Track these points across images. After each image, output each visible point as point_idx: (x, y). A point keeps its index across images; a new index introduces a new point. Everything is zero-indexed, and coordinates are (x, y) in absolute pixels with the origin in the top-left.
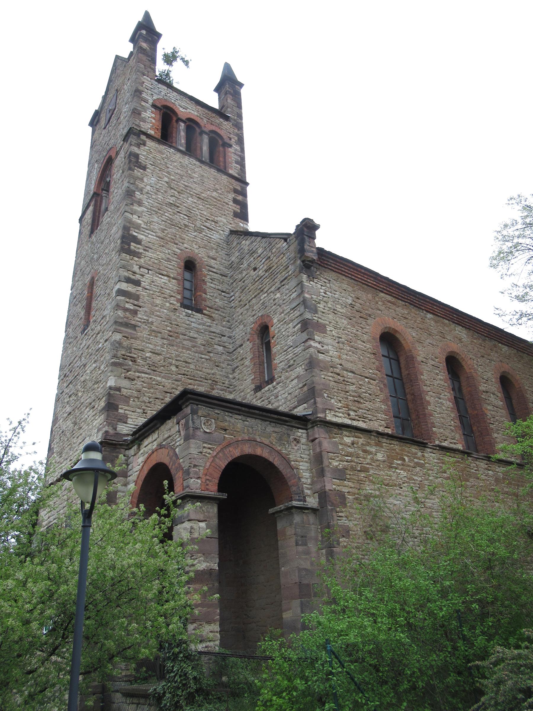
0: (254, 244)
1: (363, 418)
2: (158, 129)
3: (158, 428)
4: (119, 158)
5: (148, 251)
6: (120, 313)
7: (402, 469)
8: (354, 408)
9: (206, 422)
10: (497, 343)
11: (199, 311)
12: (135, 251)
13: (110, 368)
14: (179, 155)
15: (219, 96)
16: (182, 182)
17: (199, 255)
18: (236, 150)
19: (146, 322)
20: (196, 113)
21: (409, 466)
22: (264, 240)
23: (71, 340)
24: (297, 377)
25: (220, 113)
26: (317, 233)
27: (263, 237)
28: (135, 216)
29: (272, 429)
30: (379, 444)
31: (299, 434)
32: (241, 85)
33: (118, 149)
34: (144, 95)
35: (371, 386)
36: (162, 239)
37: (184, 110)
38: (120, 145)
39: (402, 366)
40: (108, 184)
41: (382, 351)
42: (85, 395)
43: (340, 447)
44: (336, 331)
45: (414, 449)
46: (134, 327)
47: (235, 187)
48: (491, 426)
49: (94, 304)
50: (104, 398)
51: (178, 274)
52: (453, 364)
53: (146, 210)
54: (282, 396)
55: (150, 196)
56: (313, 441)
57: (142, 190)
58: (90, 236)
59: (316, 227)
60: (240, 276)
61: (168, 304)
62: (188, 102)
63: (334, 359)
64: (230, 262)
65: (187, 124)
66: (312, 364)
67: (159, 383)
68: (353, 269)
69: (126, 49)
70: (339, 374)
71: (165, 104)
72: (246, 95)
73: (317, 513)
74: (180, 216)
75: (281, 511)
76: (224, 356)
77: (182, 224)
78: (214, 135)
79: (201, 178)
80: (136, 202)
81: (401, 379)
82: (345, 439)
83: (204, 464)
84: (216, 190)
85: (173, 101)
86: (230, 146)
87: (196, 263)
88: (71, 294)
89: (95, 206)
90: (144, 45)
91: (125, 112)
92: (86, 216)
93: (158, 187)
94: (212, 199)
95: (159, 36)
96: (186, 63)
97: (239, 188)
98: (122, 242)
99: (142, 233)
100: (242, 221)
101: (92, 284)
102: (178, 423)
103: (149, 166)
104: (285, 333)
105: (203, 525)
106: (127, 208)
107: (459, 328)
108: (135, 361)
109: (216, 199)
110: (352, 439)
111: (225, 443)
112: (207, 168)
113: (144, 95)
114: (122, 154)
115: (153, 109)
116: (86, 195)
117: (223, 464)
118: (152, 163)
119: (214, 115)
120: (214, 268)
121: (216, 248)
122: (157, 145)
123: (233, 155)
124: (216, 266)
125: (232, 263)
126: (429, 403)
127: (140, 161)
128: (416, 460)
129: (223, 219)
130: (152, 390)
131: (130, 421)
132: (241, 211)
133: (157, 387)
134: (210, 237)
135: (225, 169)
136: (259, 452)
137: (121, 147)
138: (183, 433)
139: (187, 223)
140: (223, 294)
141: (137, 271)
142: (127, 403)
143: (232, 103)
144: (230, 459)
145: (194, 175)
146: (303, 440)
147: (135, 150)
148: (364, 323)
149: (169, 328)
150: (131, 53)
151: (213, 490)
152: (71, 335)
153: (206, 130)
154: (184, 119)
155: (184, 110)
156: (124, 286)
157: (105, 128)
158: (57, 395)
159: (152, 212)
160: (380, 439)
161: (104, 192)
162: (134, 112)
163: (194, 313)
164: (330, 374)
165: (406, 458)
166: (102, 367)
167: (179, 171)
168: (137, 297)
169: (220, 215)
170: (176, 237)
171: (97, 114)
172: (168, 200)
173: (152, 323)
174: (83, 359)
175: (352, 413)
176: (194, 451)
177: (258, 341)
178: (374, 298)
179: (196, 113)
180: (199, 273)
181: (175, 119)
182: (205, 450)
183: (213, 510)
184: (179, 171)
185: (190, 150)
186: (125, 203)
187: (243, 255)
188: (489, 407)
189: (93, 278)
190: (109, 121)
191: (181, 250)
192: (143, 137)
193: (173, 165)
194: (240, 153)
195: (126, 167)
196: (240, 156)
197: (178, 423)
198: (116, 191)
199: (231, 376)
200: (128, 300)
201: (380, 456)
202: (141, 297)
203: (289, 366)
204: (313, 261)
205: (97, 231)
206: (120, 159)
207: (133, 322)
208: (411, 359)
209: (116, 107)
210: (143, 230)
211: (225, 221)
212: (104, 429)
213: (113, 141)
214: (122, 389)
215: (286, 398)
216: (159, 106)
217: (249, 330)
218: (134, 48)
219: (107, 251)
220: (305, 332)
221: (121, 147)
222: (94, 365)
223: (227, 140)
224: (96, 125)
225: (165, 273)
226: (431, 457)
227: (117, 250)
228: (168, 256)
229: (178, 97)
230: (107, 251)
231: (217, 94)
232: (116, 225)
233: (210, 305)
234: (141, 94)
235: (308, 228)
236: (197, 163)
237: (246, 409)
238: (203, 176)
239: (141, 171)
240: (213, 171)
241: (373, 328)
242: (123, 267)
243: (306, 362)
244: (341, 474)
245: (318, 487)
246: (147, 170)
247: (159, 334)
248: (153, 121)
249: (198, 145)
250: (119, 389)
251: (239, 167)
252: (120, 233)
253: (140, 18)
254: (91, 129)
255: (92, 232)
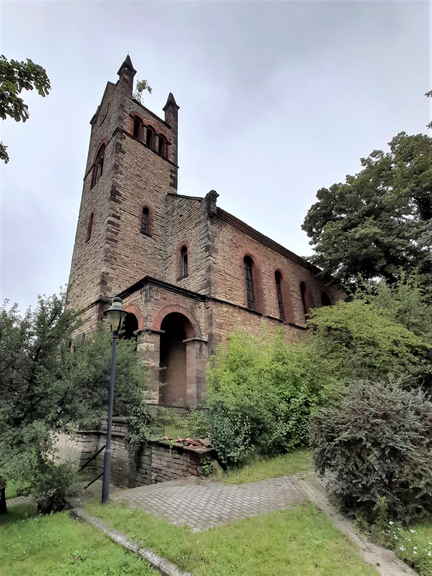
0: (182, 202)
1: (233, 299)
3: (129, 295)
4: (109, 145)
6: (110, 233)
7: (249, 326)
8: (229, 294)
9: (158, 294)
10: (301, 266)
11: (150, 236)
13: (103, 262)
14: (142, 147)
15: (165, 113)
18: (173, 147)
19: (122, 239)
20: (153, 123)
21: (253, 325)
22: (187, 200)
23: (79, 246)
24: (201, 275)
25: (165, 124)
26: (218, 199)
27: (187, 199)
28: (118, 180)
29: (188, 301)
30: (239, 313)
31: (201, 304)
32: (178, 108)
35: (238, 283)
37: (148, 121)
39: (253, 274)
40: (102, 160)
41: (243, 265)
42: (88, 275)
43: (221, 312)
44: (223, 252)
45: (256, 317)
46: (116, 241)
48: (294, 309)
49: (93, 227)
50: (100, 278)
51: (140, 215)
52: (278, 275)
54: (193, 284)
56: (207, 308)
58: (91, 189)
59: (218, 195)
60: (172, 219)
61: (134, 231)
63: (221, 268)
66: (209, 269)
67: (128, 272)
68: (234, 220)
69: (115, 79)
70: (222, 276)
72: (182, 115)
73: (207, 344)
75: (189, 342)
76: (161, 261)
81: (252, 281)
82: (224, 308)
83: (155, 315)
84: (161, 169)
86: (170, 144)
88: (79, 220)
89: (94, 172)
90: (126, 77)
92: (88, 177)
95: (135, 72)
96: (150, 90)
97: (174, 170)
98: (111, 194)
101: (92, 216)
102: (141, 294)
103: (126, 152)
104: (196, 252)
105: (152, 345)
107: (283, 257)
108: (116, 260)
110: (227, 309)
111: (164, 306)
112: (157, 156)
113: (125, 108)
114: (111, 143)
117: (163, 316)
119: (162, 124)
123: (171, 149)
124: (159, 212)
126: (265, 294)
128: (256, 322)
130: (124, 276)
131: (112, 291)
133: (127, 274)
136: (181, 311)
137: (111, 139)
138: (143, 299)
139: (145, 187)
140: (162, 228)
141: (119, 211)
142: (112, 282)
143: (173, 118)
144: (167, 314)
146: (203, 308)
147: (120, 142)
148: (237, 250)
149: (134, 244)
150: (118, 82)
151: (158, 328)
152: (79, 243)
154: (146, 125)
155: (147, 120)
156: (112, 219)
157: (100, 126)
158: (70, 274)
160: (240, 310)
163: (147, 237)
164: (219, 275)
165: (252, 321)
166: (98, 261)
168: (118, 226)
171: (95, 117)
173: (125, 240)
174: (86, 256)
175: (228, 296)
176: (149, 308)
177: (180, 255)
178: (243, 237)
179: (153, 123)
180: (150, 215)
181: (141, 125)
182: (155, 308)
183: (157, 338)
185: (149, 145)
187: (175, 208)
188: (293, 299)
189: (93, 213)
192: (124, 134)
197: (141, 294)
198: (107, 164)
199: (164, 272)
200: (113, 227)
201: (239, 319)
202: (120, 226)
203: (197, 269)
204: (214, 214)
207: (116, 239)
208: (258, 271)
212: (100, 294)
214: (110, 274)
215: (194, 285)
216: (133, 115)
217: (175, 248)
218: (120, 78)
219: (101, 198)
220: (207, 252)
221: (111, 139)
222: (94, 260)
223: (169, 141)
224: (94, 124)
225: (133, 214)
226: (264, 321)
229: (144, 112)
233: (155, 233)
235: (213, 196)
236: (152, 152)
237: (176, 289)
238: (155, 160)
240: (160, 158)
241: (241, 254)
242: (112, 208)
243: (207, 268)
244: (220, 326)
245: (209, 331)
247: (129, 247)
248: (130, 125)
249: (153, 141)
250: (108, 274)
252: (110, 189)
253: (124, 59)
254: (91, 126)
255: (92, 187)
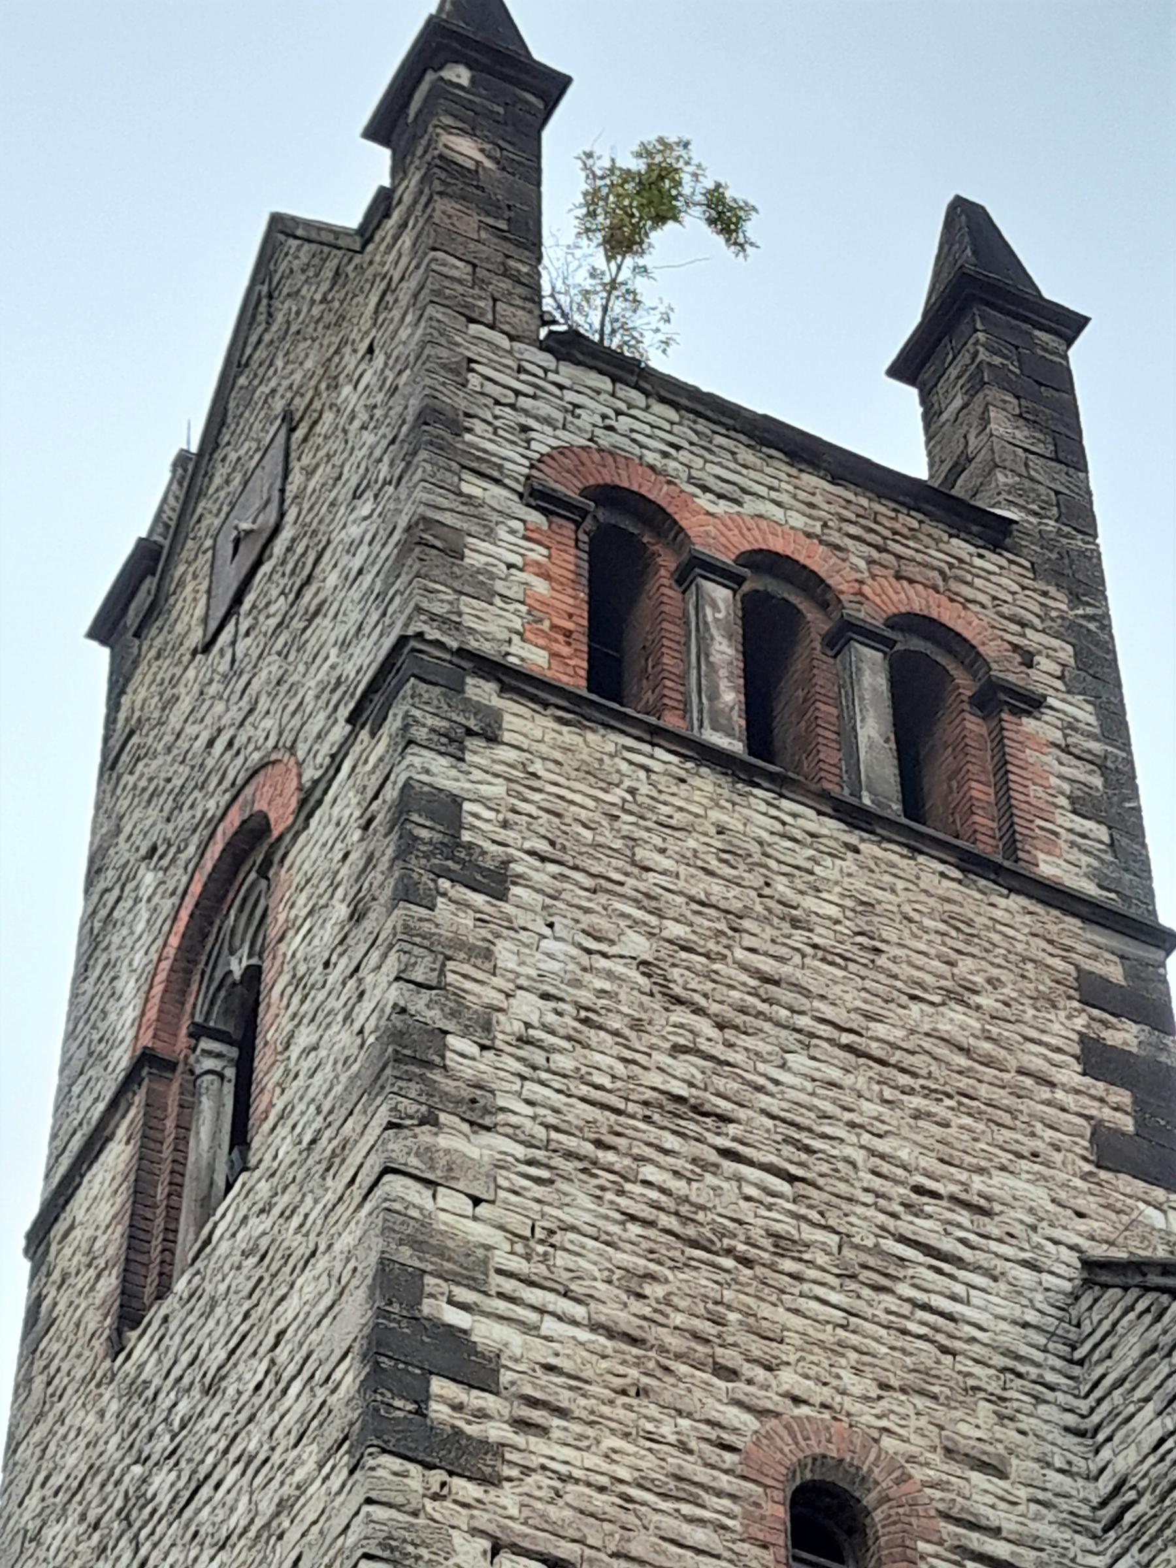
2: (568, 634)
4: (320, 827)
5: (543, 1431)
12: (458, 1432)
14: (706, 783)
15: (924, 400)
16: (740, 954)
17: (887, 1442)
18: (1071, 726)
25: (941, 503)
28: (446, 1198)
33: (310, 774)
34: (479, 437)
36: (634, 1341)
37: (735, 511)
38: (326, 748)
47: (1088, 965)
53: (520, 1151)
55: (539, 1057)
57: (487, 1027)
58: (117, 1346)
62: (746, 455)
64: (1105, 1485)
65: (746, 587)
69: (345, 181)
71: (608, 476)
74: (739, 1179)
77: (756, 1233)
78: (917, 644)
79: (861, 922)
80: (457, 1104)
84: (960, 994)
85: (651, 457)
86: (1033, 704)
87: (869, 1500)
90: (466, 148)
91: (352, 549)
93: (585, 997)
94: (942, 1051)
97: (1115, 973)
98: (374, 1380)
99: (502, 1306)
100: (1159, 1194)
106: (398, 1148)
109: (965, 1051)
112: (893, 854)
113: (479, 437)
114: (343, 803)
115: (535, 517)
116: (73, 1073)
118: (542, 846)
120: (996, 1532)
121: (994, 1387)
122: (569, 736)
123: (1050, 759)
124: (1007, 1521)
125: (1116, 1491)
127: (466, 836)
129: (1019, 1188)
132: (1137, 1123)
134: (950, 1317)
135: (1012, 846)
137: (336, 761)
139: (786, 1226)
143: (1021, 435)
145: (810, 902)
147: (441, 772)
150: (383, 203)
153: (870, 615)
159: (557, 1161)
161: (206, 1044)
162: (422, 543)
167: (717, 889)
169: (1005, 1158)
170: (718, 1321)
171: (149, 565)
172: (657, 1079)
181: (667, 562)
184: (717, 889)
185: (767, 754)
186: (383, 1115)
190: (238, 600)
191: (761, 1413)
192: (482, 691)
193: (672, 846)
194: (1096, 746)
195: (382, 882)
196: (1100, 765)
198: (305, 1037)
205: (169, 1304)
206: (330, 832)
209: (282, 515)
210: (509, 1286)
211: (1039, 1195)
213: (268, 723)
216: (569, 489)
219: (253, 1441)
221: (336, 761)
227: (333, 1433)
228: (676, 1460)
230: (253, 1441)
231: (912, 393)
232: (321, 1263)
234: (459, 431)
236: (830, 827)
239: (479, 899)
240: (931, 875)
246: (515, 890)
248: (541, 587)
251: (1103, 833)
252: (355, 1314)
254: (102, 655)
255: (129, 1314)
